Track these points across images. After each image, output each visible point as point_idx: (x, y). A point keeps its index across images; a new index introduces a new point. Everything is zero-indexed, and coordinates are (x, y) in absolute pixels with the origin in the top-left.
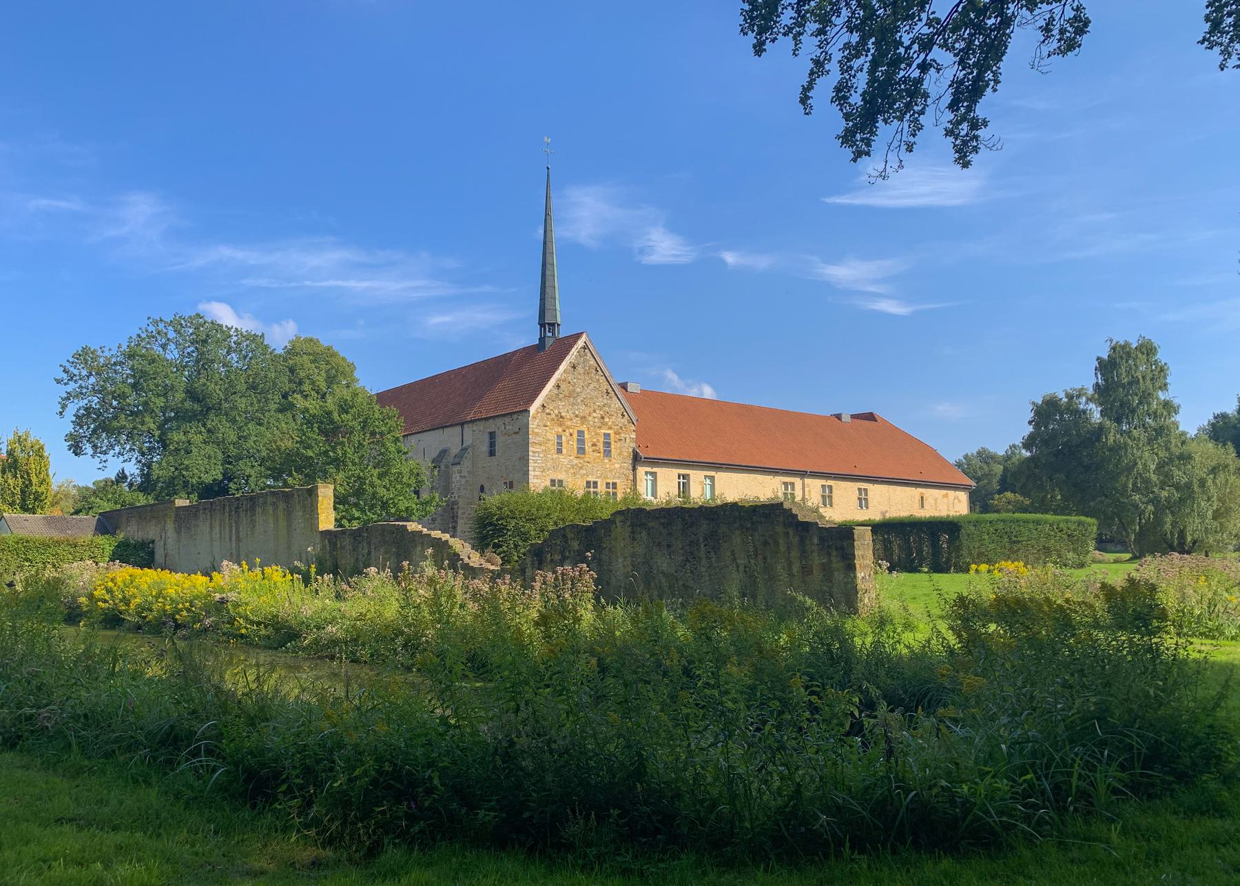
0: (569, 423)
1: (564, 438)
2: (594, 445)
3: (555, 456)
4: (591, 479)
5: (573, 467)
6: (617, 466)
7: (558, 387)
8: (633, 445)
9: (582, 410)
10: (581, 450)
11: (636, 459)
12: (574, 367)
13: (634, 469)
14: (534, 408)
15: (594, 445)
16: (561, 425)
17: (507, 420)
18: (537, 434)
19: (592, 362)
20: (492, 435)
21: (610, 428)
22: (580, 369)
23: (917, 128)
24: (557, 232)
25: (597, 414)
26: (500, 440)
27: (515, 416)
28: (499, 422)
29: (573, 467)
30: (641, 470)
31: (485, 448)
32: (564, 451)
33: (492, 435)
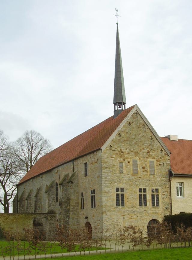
0: (127, 156)
1: (124, 164)
2: (144, 168)
3: (118, 175)
4: (142, 187)
5: (130, 180)
6: (159, 179)
7: (120, 135)
8: (169, 167)
9: (135, 148)
10: (135, 173)
11: (171, 175)
12: (130, 124)
13: (170, 181)
14: (104, 148)
15: (144, 168)
16: (122, 157)
17: (92, 155)
18: (107, 162)
19: (141, 121)
20: (86, 164)
21: (154, 158)
22: (133, 125)
23: (46, 176)
24: (60, 168)
25: (146, 150)
26: (89, 167)
27: (95, 153)
28: (88, 157)
29: (130, 180)
30: (175, 183)
31: (83, 173)
32: (125, 172)
33: (86, 164)
